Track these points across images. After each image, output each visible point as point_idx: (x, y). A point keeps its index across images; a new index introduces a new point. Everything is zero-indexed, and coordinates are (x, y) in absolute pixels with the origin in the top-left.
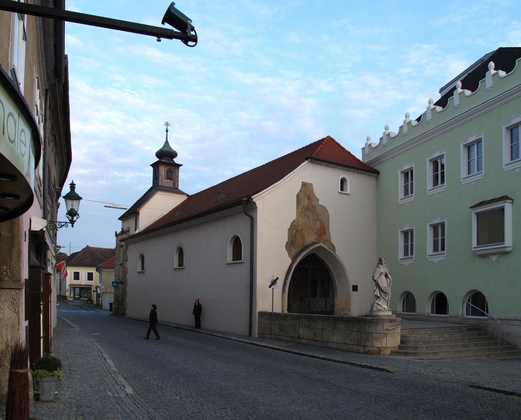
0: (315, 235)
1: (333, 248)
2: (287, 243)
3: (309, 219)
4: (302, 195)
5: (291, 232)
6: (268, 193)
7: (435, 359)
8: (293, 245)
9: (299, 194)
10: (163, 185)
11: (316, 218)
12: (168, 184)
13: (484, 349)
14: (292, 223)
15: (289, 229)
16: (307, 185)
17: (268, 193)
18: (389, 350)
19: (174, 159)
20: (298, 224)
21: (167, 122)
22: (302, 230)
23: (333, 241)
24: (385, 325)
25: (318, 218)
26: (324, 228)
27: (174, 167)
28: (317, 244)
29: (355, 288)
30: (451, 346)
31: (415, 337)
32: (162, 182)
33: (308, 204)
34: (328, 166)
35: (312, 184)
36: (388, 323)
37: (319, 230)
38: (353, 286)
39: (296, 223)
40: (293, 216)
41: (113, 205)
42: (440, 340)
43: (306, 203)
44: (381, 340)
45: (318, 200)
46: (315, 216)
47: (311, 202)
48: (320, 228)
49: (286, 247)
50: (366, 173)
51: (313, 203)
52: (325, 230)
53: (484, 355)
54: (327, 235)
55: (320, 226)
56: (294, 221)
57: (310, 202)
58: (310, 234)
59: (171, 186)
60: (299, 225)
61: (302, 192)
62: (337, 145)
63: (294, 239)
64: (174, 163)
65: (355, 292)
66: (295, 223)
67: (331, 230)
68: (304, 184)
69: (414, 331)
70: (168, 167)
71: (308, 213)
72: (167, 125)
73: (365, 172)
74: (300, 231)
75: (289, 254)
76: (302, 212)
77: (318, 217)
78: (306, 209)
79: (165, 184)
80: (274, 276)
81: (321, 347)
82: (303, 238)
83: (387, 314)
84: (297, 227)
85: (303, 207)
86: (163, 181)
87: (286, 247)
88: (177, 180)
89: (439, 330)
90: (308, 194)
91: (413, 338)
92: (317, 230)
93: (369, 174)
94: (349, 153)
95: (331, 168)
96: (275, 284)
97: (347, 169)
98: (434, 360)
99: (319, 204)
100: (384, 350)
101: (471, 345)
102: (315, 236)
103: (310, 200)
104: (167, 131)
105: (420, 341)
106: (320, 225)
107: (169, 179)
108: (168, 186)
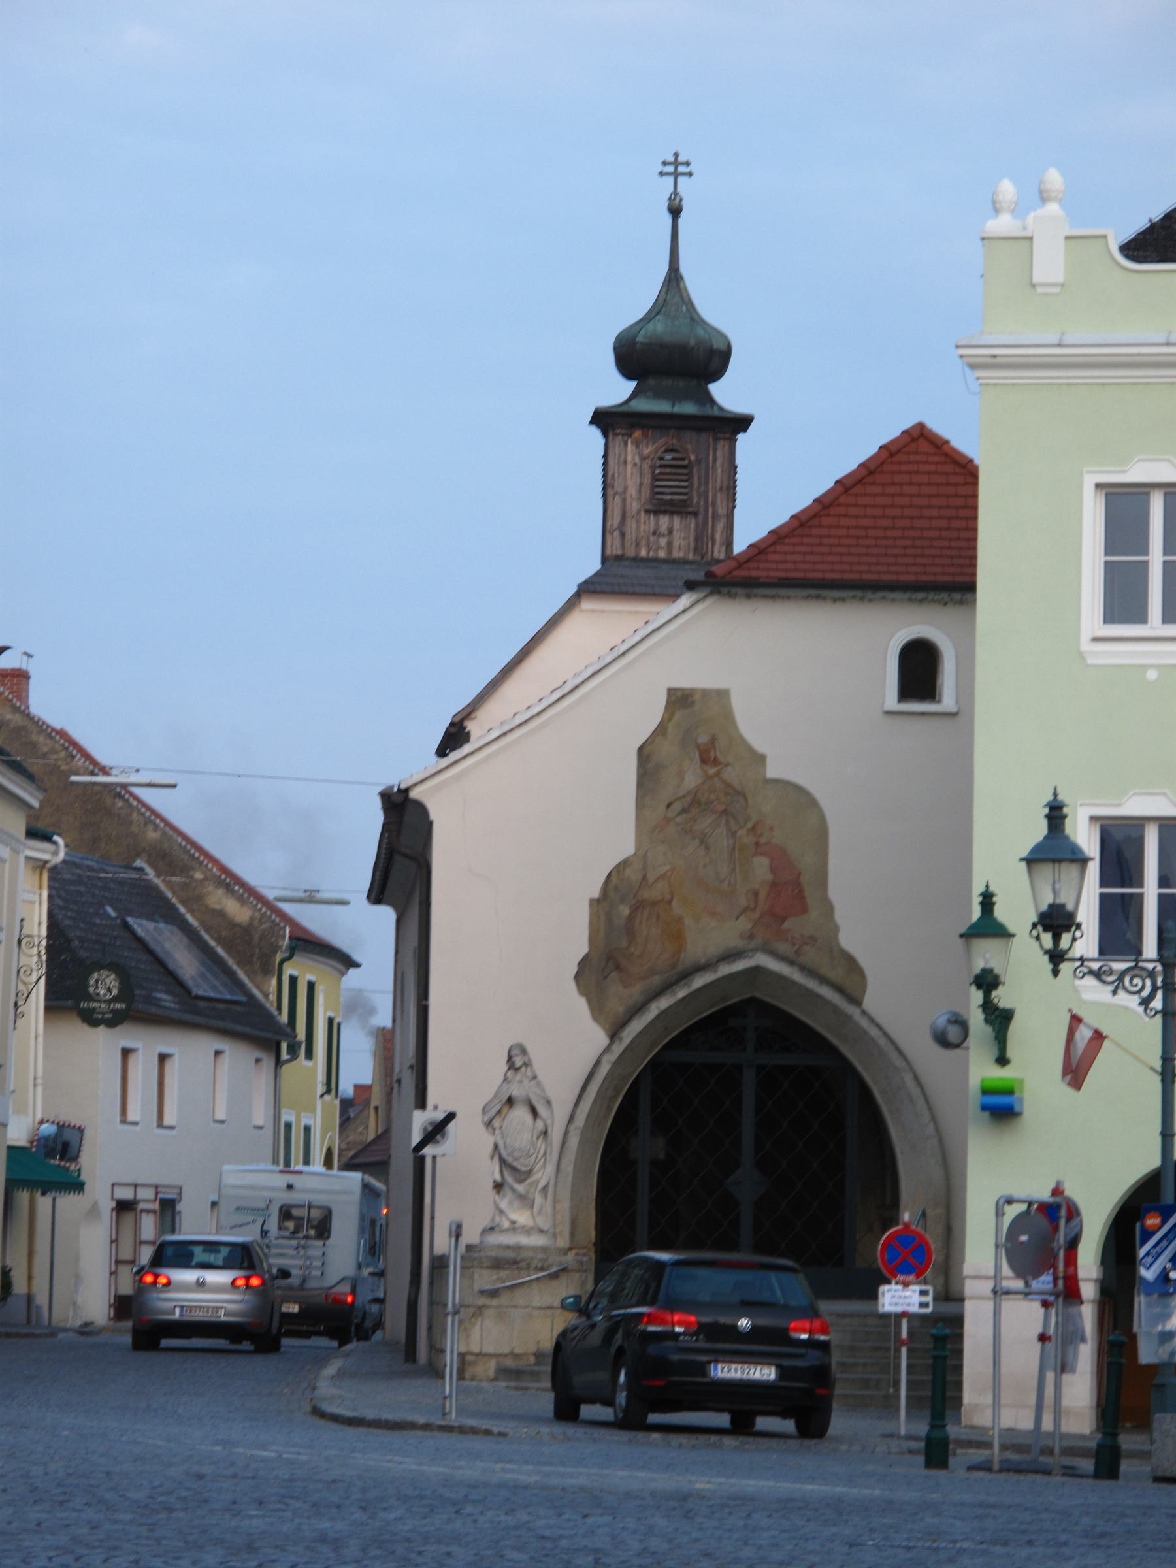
0: (742, 918)
2: (584, 963)
3: (707, 848)
6: (486, 759)
8: (618, 967)
9: (653, 742)
10: (631, 553)
11: (749, 840)
12: (663, 542)
14: (609, 875)
15: (595, 903)
16: (697, 697)
17: (486, 759)
18: (492, 1364)
19: (715, 389)
20: (645, 877)
21: (676, 155)
22: (668, 897)
23: (848, 940)
26: (797, 884)
27: (704, 436)
28: (735, 960)
32: (623, 535)
33: (704, 783)
34: (818, 597)
35: (722, 695)
36: (485, 1272)
39: (632, 874)
43: (692, 778)
45: (761, 759)
47: (718, 774)
48: (774, 884)
51: (731, 775)
52: (801, 891)
55: (769, 877)
56: (624, 864)
57: (712, 771)
59: (676, 554)
61: (670, 730)
62: (949, 468)
63: (624, 944)
64: (716, 412)
66: (628, 872)
67: (834, 892)
70: (662, 441)
71: (704, 824)
72: (676, 175)
74: (654, 904)
75: (597, 1010)
77: (761, 835)
78: (694, 803)
79: (643, 543)
80: (440, 1108)
82: (677, 936)
86: (631, 526)
87: (578, 977)
88: (722, 511)
90: (703, 739)
92: (756, 894)
97: (936, 598)
102: (744, 924)
103: (716, 762)
104: (675, 211)
106: (773, 869)
107: (672, 513)
108: (662, 554)
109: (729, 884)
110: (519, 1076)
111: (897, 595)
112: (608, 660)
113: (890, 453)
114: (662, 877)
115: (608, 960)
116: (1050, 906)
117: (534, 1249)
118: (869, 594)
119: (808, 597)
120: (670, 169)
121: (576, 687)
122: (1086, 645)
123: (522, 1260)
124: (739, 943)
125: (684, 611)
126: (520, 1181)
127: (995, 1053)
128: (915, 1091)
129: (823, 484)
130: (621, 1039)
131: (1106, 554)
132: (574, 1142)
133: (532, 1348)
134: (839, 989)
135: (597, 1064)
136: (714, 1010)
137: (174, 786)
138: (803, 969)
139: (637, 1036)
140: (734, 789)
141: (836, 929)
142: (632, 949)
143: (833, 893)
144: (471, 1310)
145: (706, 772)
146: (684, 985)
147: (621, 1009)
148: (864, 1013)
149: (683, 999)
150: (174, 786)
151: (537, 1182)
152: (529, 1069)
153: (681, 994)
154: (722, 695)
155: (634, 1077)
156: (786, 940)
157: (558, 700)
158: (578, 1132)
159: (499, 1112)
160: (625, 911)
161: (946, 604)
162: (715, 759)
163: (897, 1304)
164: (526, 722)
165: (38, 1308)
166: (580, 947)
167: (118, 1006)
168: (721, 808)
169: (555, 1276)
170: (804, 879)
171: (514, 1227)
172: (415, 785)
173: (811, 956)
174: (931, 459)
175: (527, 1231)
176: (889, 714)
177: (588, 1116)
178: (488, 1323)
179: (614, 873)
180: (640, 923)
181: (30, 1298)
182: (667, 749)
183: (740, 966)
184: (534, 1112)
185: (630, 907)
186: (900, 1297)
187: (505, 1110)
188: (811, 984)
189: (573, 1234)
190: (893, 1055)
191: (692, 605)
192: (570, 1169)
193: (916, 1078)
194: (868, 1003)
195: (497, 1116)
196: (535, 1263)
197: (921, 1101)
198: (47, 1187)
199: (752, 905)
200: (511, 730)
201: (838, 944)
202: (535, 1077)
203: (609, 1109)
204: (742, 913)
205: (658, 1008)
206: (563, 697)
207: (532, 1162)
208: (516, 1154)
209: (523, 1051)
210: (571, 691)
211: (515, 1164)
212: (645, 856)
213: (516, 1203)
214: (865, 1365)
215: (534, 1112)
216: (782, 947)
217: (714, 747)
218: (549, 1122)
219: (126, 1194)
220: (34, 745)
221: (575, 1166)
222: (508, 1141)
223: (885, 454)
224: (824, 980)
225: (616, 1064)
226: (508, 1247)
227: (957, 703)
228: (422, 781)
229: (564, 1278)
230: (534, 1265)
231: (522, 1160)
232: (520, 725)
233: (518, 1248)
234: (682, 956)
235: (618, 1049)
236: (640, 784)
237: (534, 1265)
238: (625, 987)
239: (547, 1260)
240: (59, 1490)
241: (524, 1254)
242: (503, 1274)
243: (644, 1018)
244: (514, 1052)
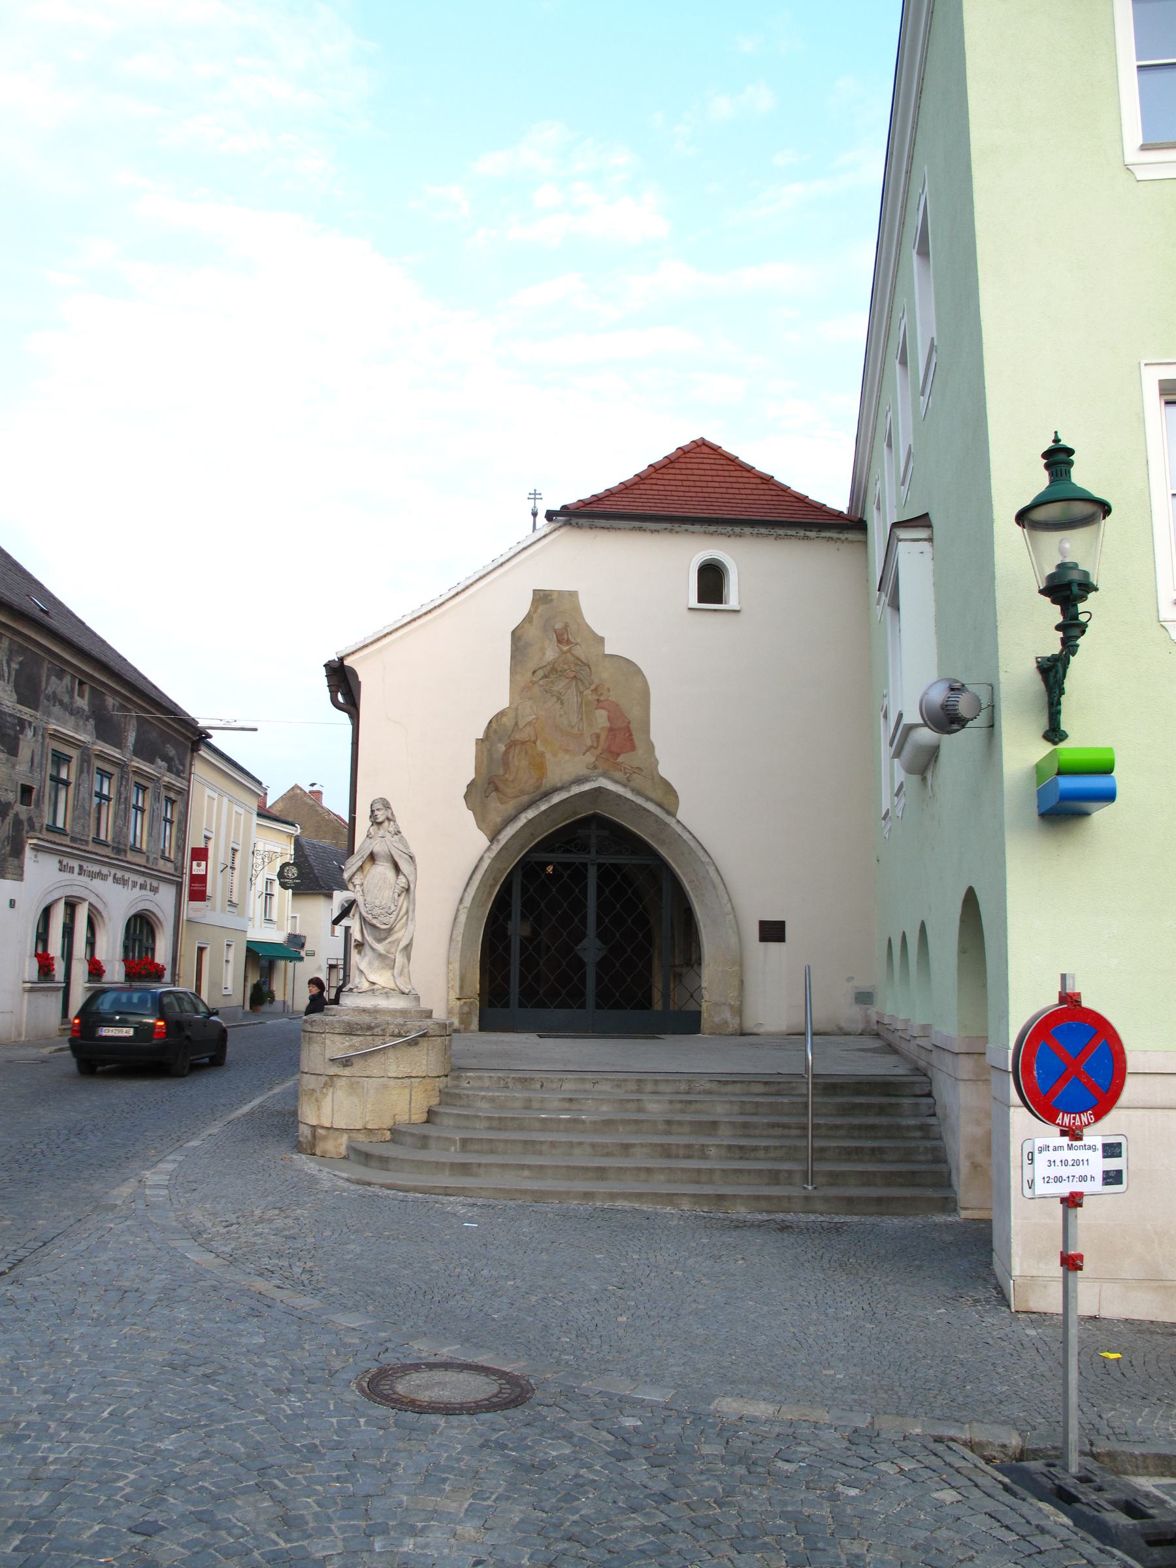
1: (668, 796)
2: (471, 786)
3: (562, 703)
4: (533, 632)
5: (489, 750)
7: (415, 1189)
8: (497, 789)
11: (594, 697)
13: (741, 1171)
14: (490, 722)
15: (479, 742)
16: (555, 596)
18: (344, 1139)
20: (516, 724)
21: (535, 490)
22: (533, 738)
23: (664, 771)
24: (328, 1042)
25: (602, 698)
26: (628, 730)
29: (773, 932)
30: (593, 1145)
31: (492, 1100)
33: (560, 657)
34: (640, 529)
35: (573, 595)
36: (337, 1038)
37: (603, 737)
38: (763, 925)
40: (498, 697)
41: (223, 722)
42: (583, 1122)
43: (551, 654)
44: (317, 1100)
45: (601, 640)
46: (588, 692)
47: (569, 651)
48: (611, 729)
49: (466, 797)
50: (812, 534)
51: (579, 651)
52: (631, 735)
53: (694, 1195)
54: (640, 751)
55: (608, 725)
56: (501, 714)
57: (565, 648)
58: (567, 751)
60: (521, 727)
61: (535, 620)
62: (724, 462)
63: (501, 772)
65: (773, 946)
66: (504, 719)
67: (657, 734)
68: (542, 598)
69: (526, 1079)
71: (560, 686)
73: (806, 530)
74: (523, 743)
75: (481, 821)
76: (533, 683)
77: (602, 694)
78: (552, 671)
81: (468, 1128)
82: (539, 766)
83: (369, 1006)
84: (513, 731)
85: (540, 668)
87: (466, 797)
89: (656, 1082)
90: (559, 626)
91: (484, 1105)
92: (598, 736)
93: (823, 534)
94: (767, 480)
95: (655, 534)
96: (347, 905)
97: (723, 531)
98: (407, 1191)
99: (606, 653)
100: (324, 1138)
101: (713, 1152)
102: (590, 758)
103: (568, 642)
105: (478, 1117)
106: (609, 719)
109: (579, 729)
110: (381, 833)
111: (697, 528)
112: (491, 568)
113: (683, 452)
114: (530, 723)
115: (489, 783)
116: (1059, 566)
117: (393, 1012)
118: (676, 526)
119: (634, 529)
120: (533, 496)
121: (467, 588)
122: (1132, 154)
123: (377, 1026)
124: (586, 772)
125: (545, 536)
126: (380, 941)
127: (1043, 723)
128: (717, 880)
129: (641, 467)
130: (498, 841)
131: (1138, 59)
132: (463, 918)
133: (388, 1123)
134: (660, 805)
135: (481, 859)
136: (567, 822)
137: (255, 730)
138: (633, 790)
139: (510, 839)
140: (581, 661)
141: (657, 762)
142: (507, 776)
143: (654, 737)
144: (323, 1079)
145: (561, 650)
146: (546, 801)
147: (498, 820)
148: (678, 821)
149: (545, 811)
150: (255, 730)
151: (398, 941)
152: (392, 823)
153: (544, 807)
154: (573, 595)
155: (508, 871)
156: (621, 770)
157: (454, 597)
158: (466, 910)
159: (361, 868)
160: (502, 748)
161: (729, 536)
162: (568, 640)
163: (1058, 1179)
164: (430, 611)
165: (288, 1006)
166: (468, 773)
167: (297, 881)
168: (572, 674)
169: (413, 1043)
170: (633, 726)
171: (373, 988)
172: (348, 655)
173: (638, 781)
174: (710, 456)
175: (387, 992)
176: (690, 609)
177: (473, 898)
178: (341, 1094)
179: (494, 721)
180: (513, 758)
181: (284, 1002)
182: (533, 632)
183: (587, 787)
184: (397, 869)
185: (506, 746)
186: (1065, 1163)
187: (367, 866)
188: (639, 800)
189: (462, 988)
190: (701, 853)
191: (550, 533)
192: (460, 938)
193: (717, 870)
194: (680, 815)
195: (358, 873)
196: (392, 1028)
197: (721, 886)
198: (292, 959)
199: (595, 745)
200: (419, 617)
201: (658, 773)
202: (398, 832)
203: (490, 894)
204: (587, 751)
205: (526, 818)
206: (457, 594)
207: (392, 920)
208: (376, 911)
209: (387, 806)
210: (463, 590)
211: (374, 922)
212: (517, 709)
213: (376, 963)
214: (766, 1148)
215: (397, 869)
216: (619, 775)
217: (567, 631)
218: (411, 878)
219: (334, 962)
220: (317, 811)
221: (463, 936)
222: (368, 899)
223: (681, 452)
224: (648, 799)
225: (495, 859)
226: (364, 1010)
227: (739, 603)
228: (353, 653)
229: (424, 1043)
230: (389, 1032)
231: (381, 918)
232: (426, 614)
233: (375, 1011)
234: (544, 780)
235: (496, 848)
236: (513, 657)
237: (389, 1032)
238: (501, 804)
239: (405, 1024)
240: (156, 1145)
241: (381, 1019)
242: (356, 1040)
243: (515, 825)
244: (377, 806)
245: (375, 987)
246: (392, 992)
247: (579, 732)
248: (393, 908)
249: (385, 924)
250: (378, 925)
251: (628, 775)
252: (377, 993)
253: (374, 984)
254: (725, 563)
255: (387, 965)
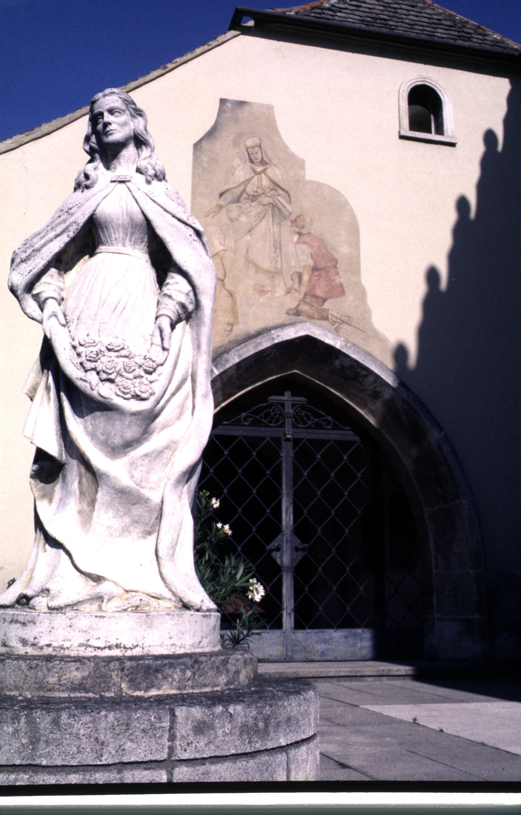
25: (304, 231)
37: (306, 278)
48: (315, 269)
77: (303, 227)
92: (300, 276)
245: (104, 588)
246: (154, 603)
247: (105, 436)
248: (158, 356)
249: (137, 397)
250: (118, 401)
251: (336, 325)
252: (109, 607)
253: (97, 579)
254: (434, 87)
255: (136, 522)
